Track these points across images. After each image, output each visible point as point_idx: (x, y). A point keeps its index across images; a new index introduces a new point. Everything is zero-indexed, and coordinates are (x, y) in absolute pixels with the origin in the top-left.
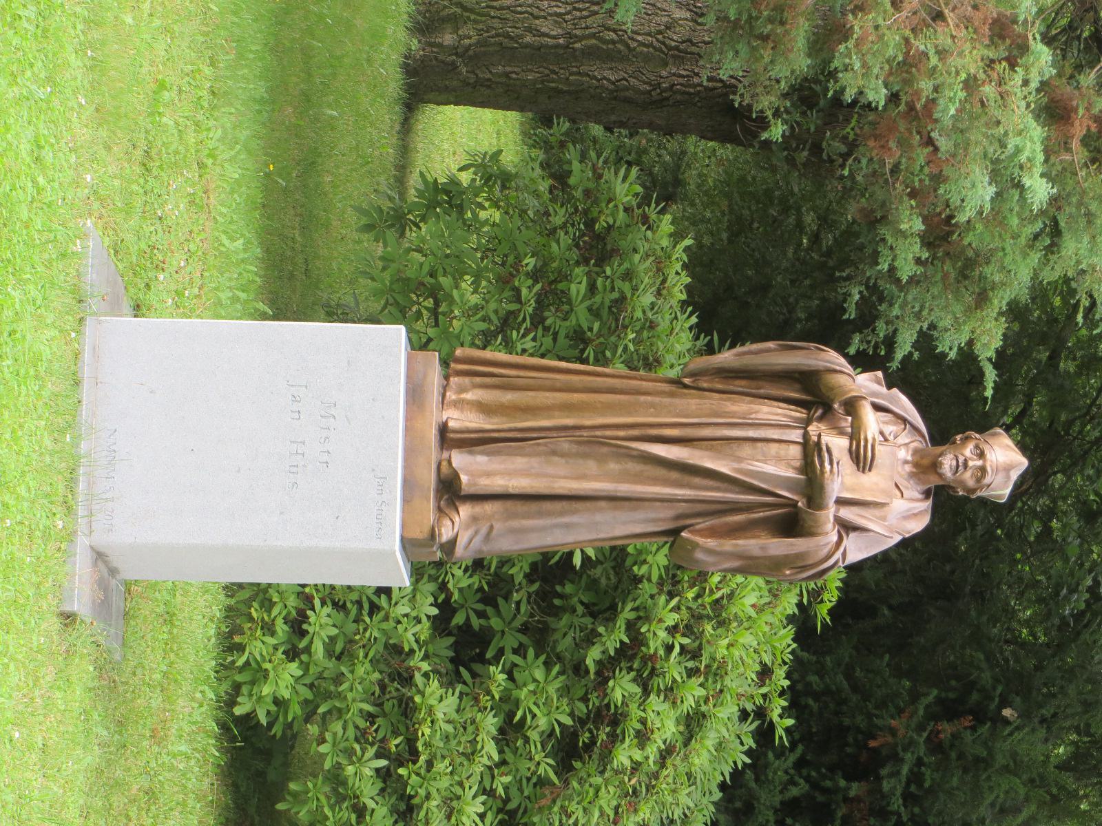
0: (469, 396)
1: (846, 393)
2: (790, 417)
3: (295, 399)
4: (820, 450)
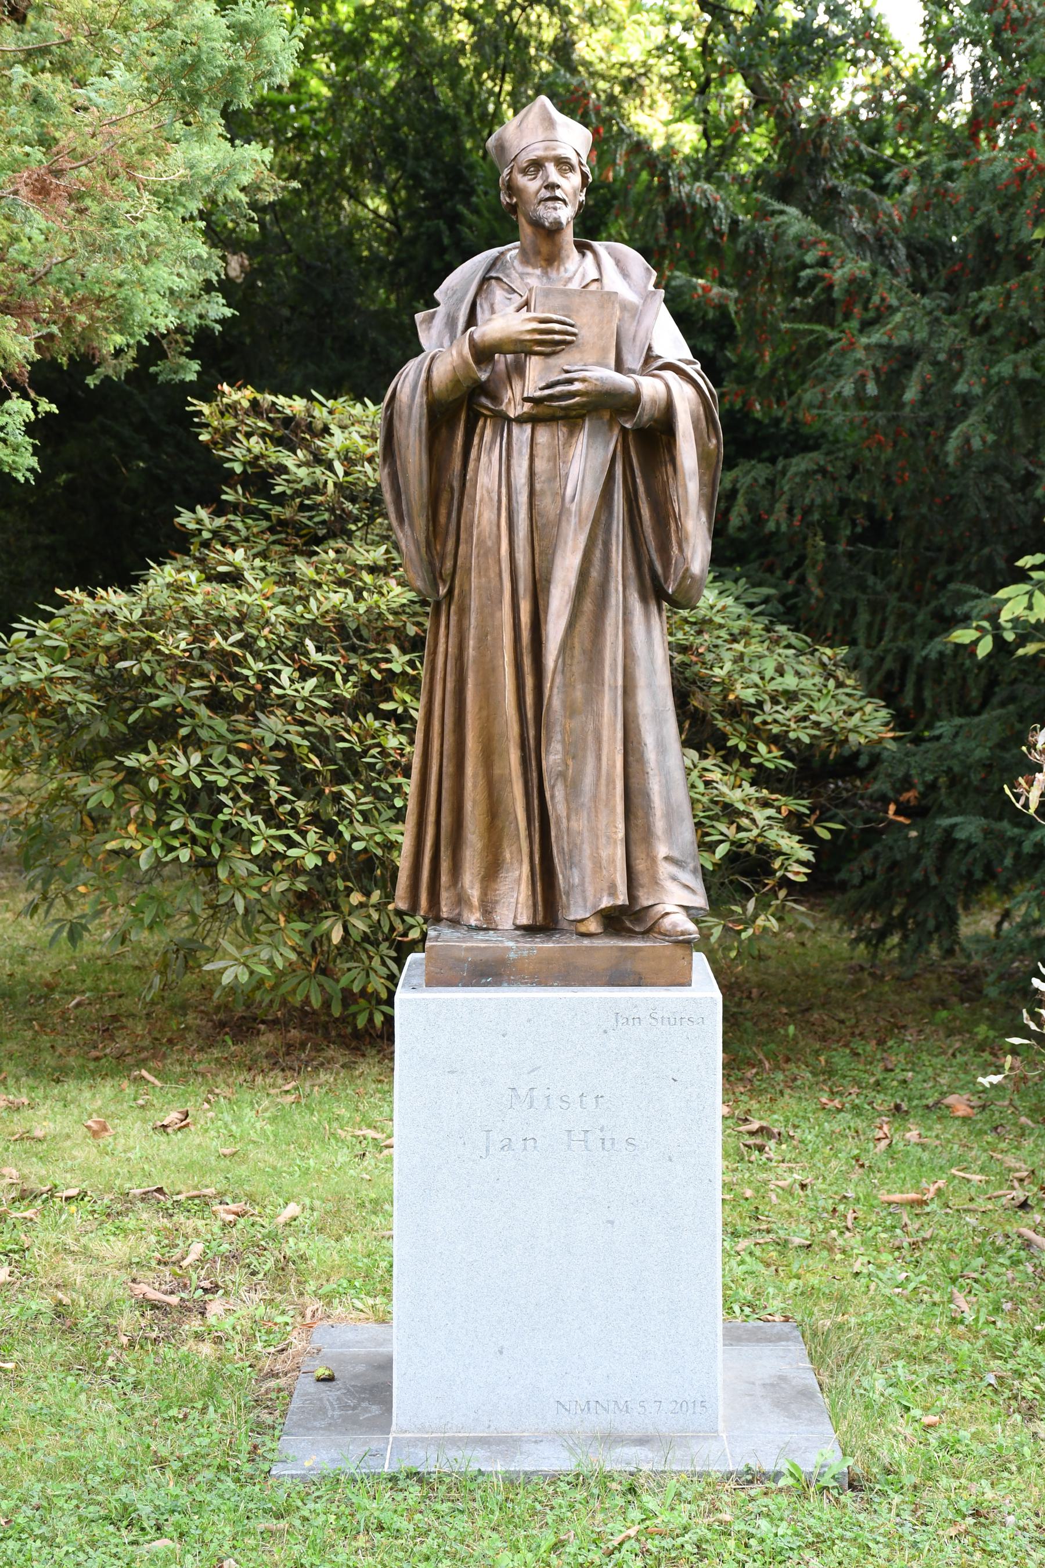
0: (474, 893)
1: (465, 362)
2: (493, 442)
3: (507, 1145)
4: (551, 398)
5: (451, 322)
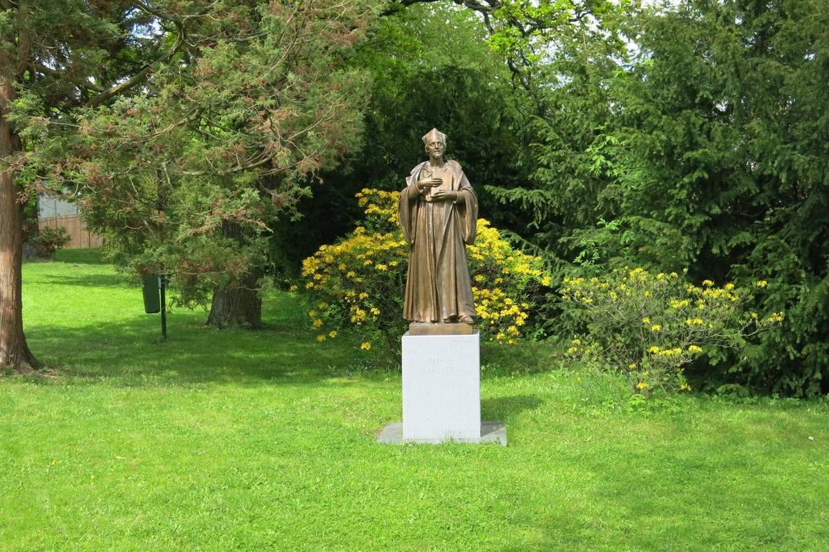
5: (414, 179)
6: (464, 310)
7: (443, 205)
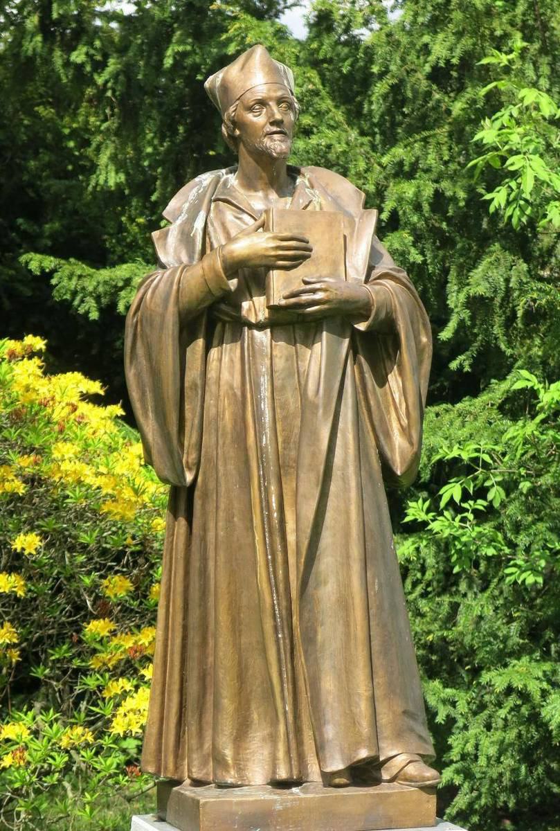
6: (399, 735)
7: (309, 340)
